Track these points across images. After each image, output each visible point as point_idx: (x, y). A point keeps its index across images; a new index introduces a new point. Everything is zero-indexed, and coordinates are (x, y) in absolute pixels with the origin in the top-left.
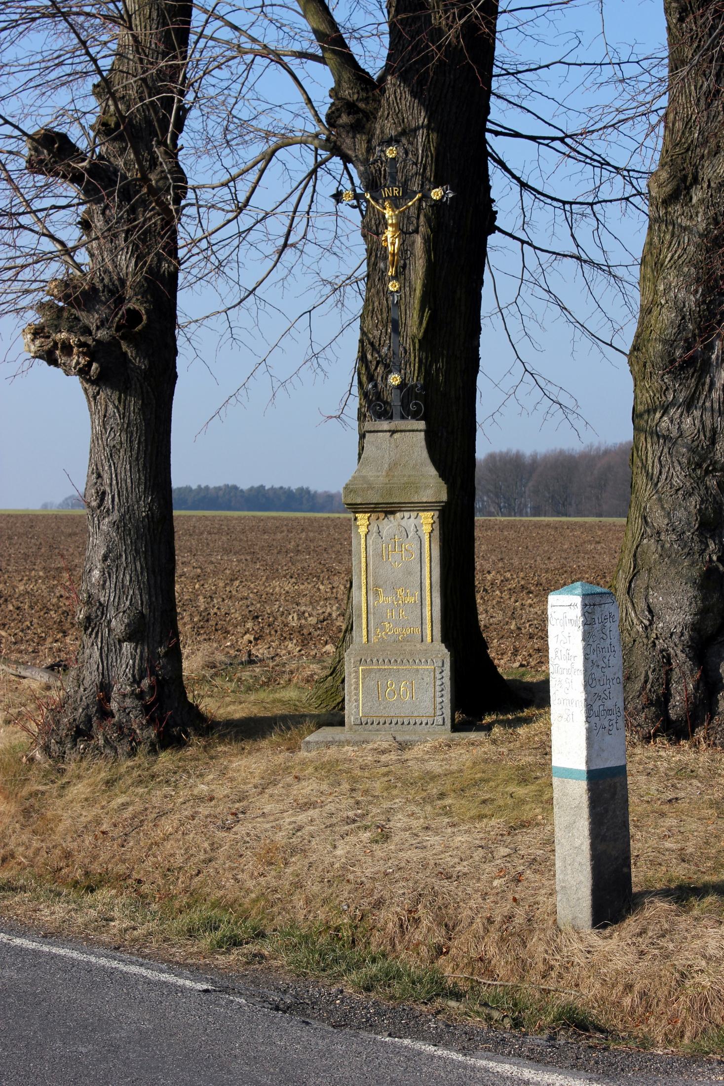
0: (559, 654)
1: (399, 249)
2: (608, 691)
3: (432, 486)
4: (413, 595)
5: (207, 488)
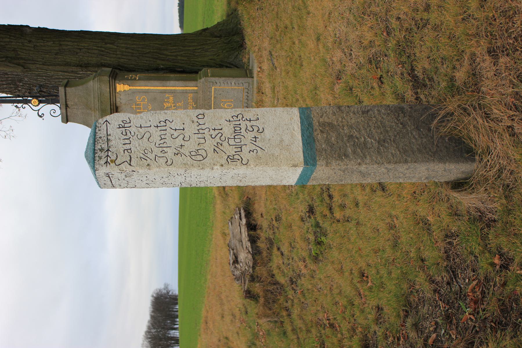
2: (212, 132)
4: (168, 98)
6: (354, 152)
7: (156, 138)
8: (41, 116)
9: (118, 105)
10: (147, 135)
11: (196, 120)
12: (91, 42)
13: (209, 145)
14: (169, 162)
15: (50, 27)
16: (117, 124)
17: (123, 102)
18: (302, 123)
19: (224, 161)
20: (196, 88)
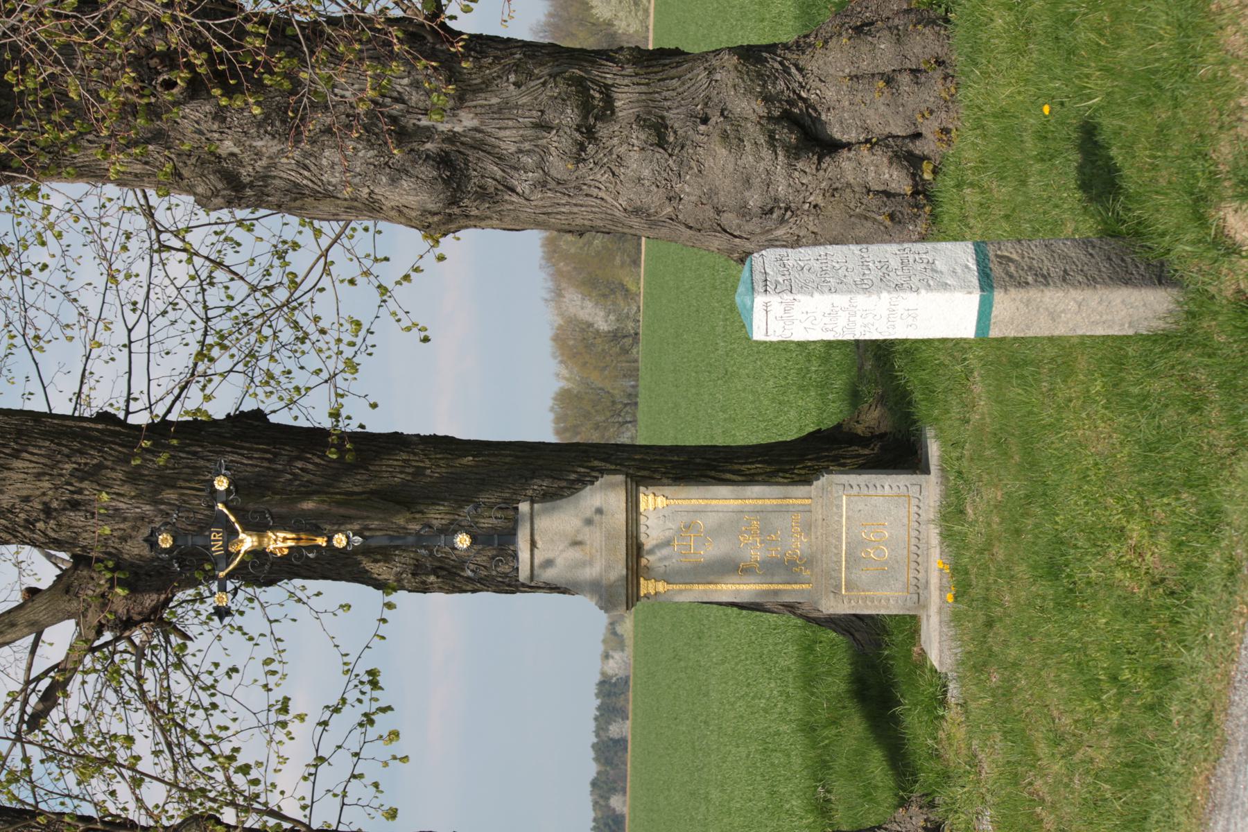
0: (830, 327)
1: (292, 531)
3: (605, 497)
5: (595, 820)
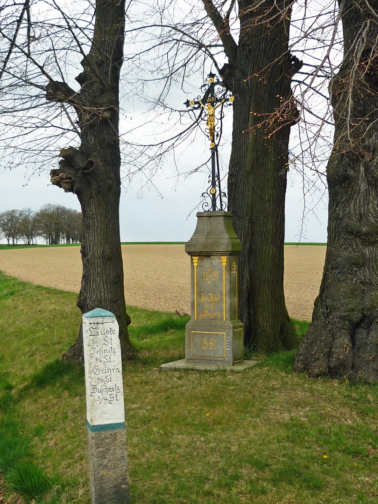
6: (100, 452)
7: (105, 347)
8: (202, 195)
9: (212, 257)
10: (107, 343)
11: (116, 368)
12: (273, 225)
13: (102, 375)
14: (92, 355)
15: (286, 194)
16: (112, 327)
17: (214, 261)
18: (116, 424)
19: (93, 384)
20: (224, 319)
